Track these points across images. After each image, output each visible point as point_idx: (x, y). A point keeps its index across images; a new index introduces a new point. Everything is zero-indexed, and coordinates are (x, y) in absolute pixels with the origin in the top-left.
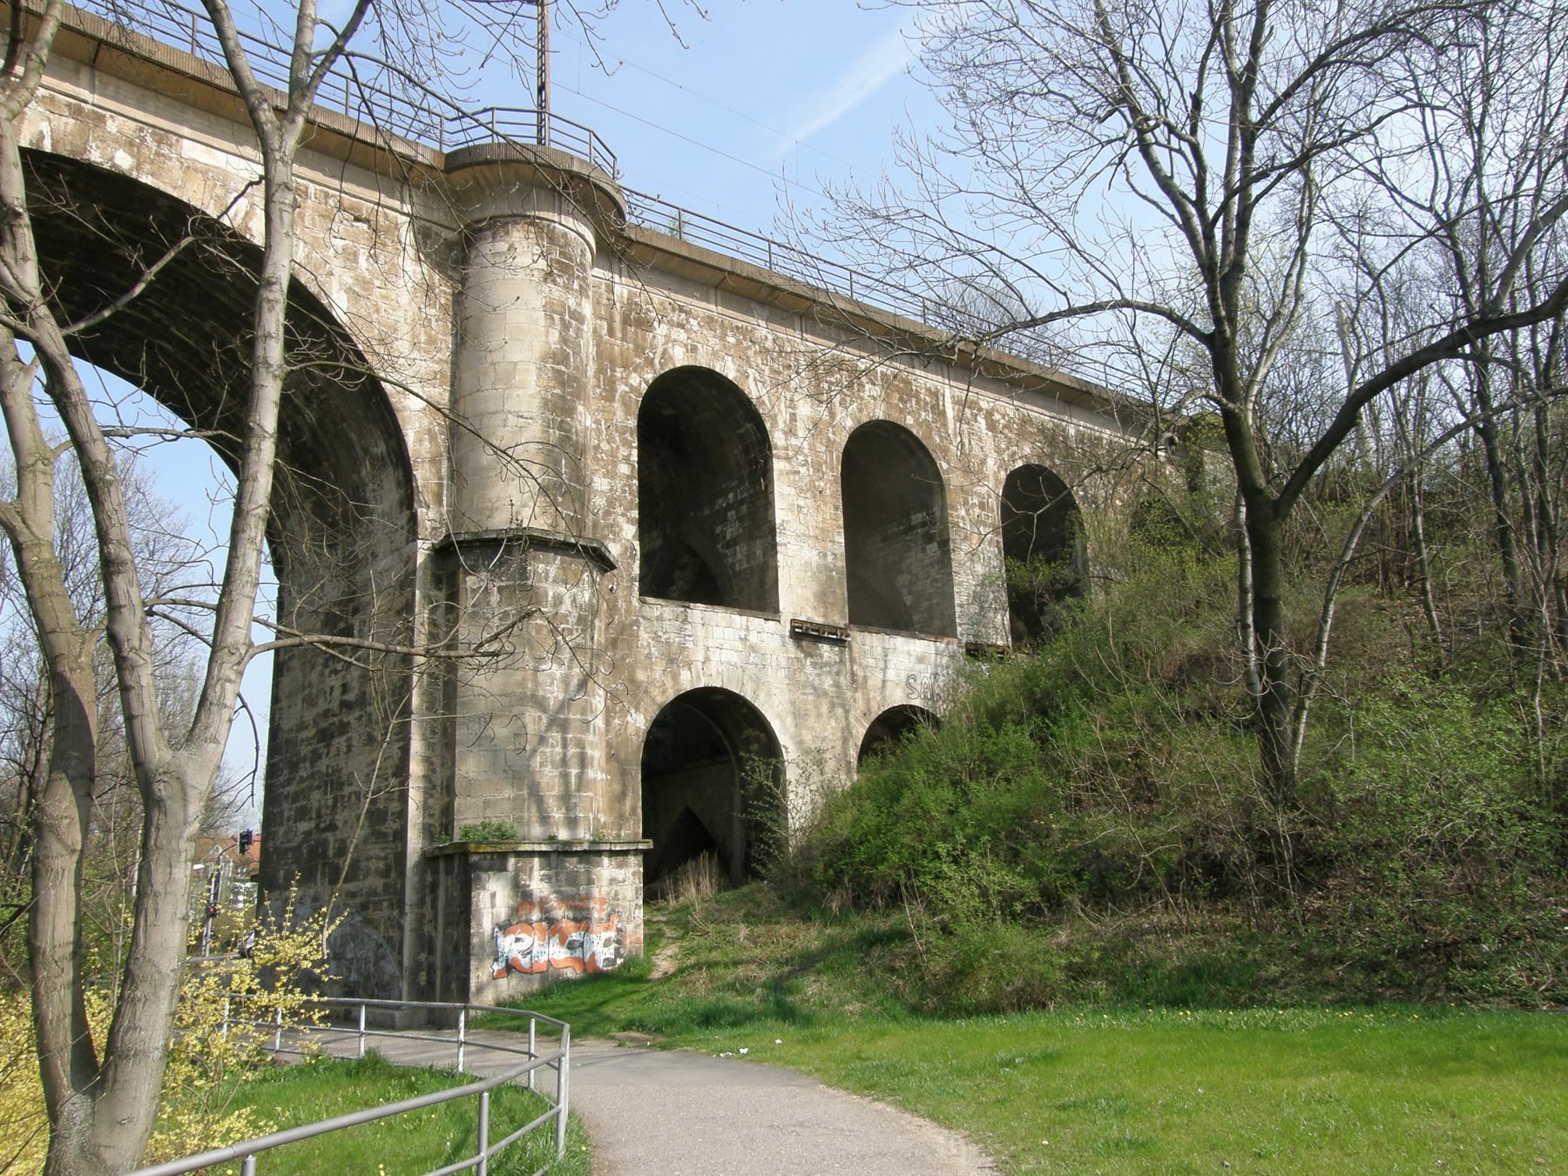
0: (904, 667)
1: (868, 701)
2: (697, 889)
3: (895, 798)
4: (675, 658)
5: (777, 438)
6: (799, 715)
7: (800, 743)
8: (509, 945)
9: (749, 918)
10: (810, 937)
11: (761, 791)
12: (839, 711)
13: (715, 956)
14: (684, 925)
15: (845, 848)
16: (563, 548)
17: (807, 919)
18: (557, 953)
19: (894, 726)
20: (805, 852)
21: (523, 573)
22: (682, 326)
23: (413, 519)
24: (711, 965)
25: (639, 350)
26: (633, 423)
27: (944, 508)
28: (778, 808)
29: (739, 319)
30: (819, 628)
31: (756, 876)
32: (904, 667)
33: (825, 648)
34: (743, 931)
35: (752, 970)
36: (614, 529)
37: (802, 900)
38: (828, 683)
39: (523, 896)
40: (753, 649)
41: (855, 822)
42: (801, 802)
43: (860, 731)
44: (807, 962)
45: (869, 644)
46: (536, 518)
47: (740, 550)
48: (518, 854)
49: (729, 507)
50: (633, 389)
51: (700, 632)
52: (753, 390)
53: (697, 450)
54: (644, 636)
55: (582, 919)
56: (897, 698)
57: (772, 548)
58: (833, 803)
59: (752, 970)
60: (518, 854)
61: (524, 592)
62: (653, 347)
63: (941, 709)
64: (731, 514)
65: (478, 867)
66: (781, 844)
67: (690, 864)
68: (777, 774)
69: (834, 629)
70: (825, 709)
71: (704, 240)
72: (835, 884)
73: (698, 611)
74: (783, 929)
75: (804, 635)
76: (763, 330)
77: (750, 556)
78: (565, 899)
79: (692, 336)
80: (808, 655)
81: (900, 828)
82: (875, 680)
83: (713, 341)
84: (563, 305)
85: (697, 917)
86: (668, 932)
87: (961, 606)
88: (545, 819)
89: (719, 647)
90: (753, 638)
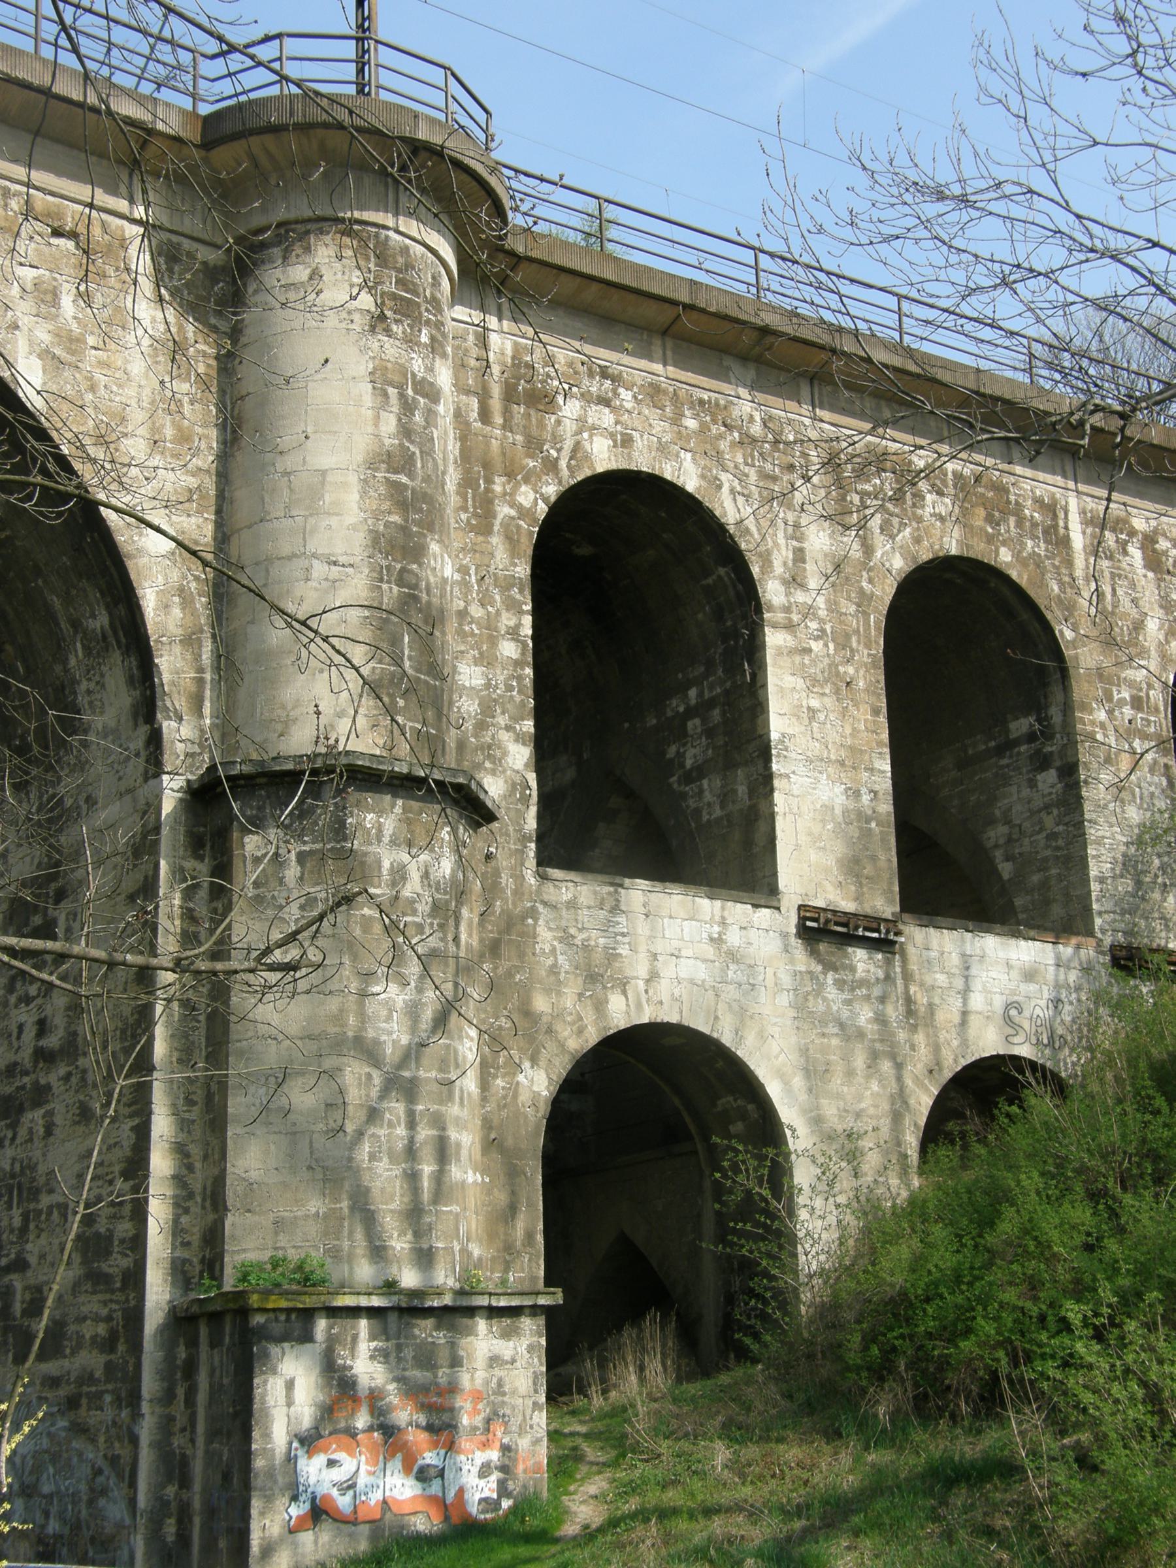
0: (998, 987)
1: (936, 1049)
2: (640, 1379)
3: (988, 1221)
4: (599, 974)
5: (772, 591)
6: (815, 1072)
7: (817, 1121)
8: (314, 1471)
9: (734, 1432)
10: (840, 1468)
11: (749, 1206)
12: (886, 1066)
13: (672, 1497)
14: (618, 1442)
15: (900, 1308)
16: (406, 785)
17: (834, 1435)
18: (400, 1488)
19: (983, 1092)
20: (829, 1314)
21: (339, 830)
22: (605, 402)
23: (155, 740)
24: (665, 1514)
25: (534, 445)
26: (523, 570)
27: (1068, 708)
28: (780, 1236)
29: (705, 387)
30: (846, 919)
31: (744, 1355)
32: (998, 987)
33: (859, 956)
34: (721, 1453)
35: (737, 1526)
36: (493, 753)
37: (824, 1400)
38: (865, 1015)
39: (340, 1386)
40: (733, 956)
41: (917, 1263)
42: (819, 1227)
43: (923, 1101)
44: (835, 1514)
45: (937, 947)
46: (362, 737)
47: (710, 787)
48: (333, 1312)
49: (690, 713)
50: (523, 513)
51: (642, 928)
52: (729, 509)
53: (635, 601)
54: (546, 936)
55: (442, 1428)
56: (988, 1042)
57: (764, 783)
58: (876, 1229)
59: (737, 1526)
60: (333, 1312)
62: (556, 440)
63: (1068, 1063)
64: (694, 725)
65: (262, 1334)
66: (785, 1300)
67: (628, 1334)
68: (778, 1175)
69: (874, 922)
70: (860, 1061)
71: (641, 251)
72: (881, 1372)
73: (639, 893)
74: (792, 1453)
75: (823, 931)
76: (747, 405)
77: (725, 797)
78: (413, 1391)
79: (623, 418)
80: (829, 966)
81: (997, 1275)
82: (948, 1013)
83: (659, 426)
84: (403, 371)
85: (640, 1425)
86: (592, 1452)
87: (1102, 880)
88: (378, 1252)
89: (672, 954)
90: (734, 938)
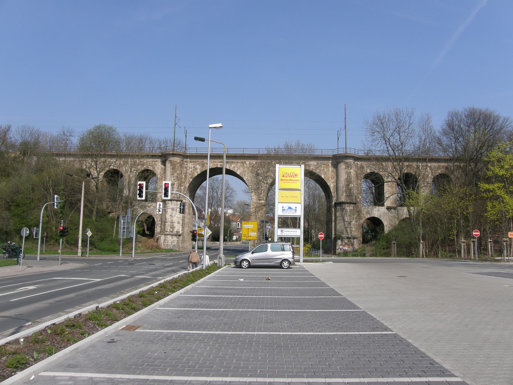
30: (390, 207)
61: (343, 210)
75: (388, 208)
